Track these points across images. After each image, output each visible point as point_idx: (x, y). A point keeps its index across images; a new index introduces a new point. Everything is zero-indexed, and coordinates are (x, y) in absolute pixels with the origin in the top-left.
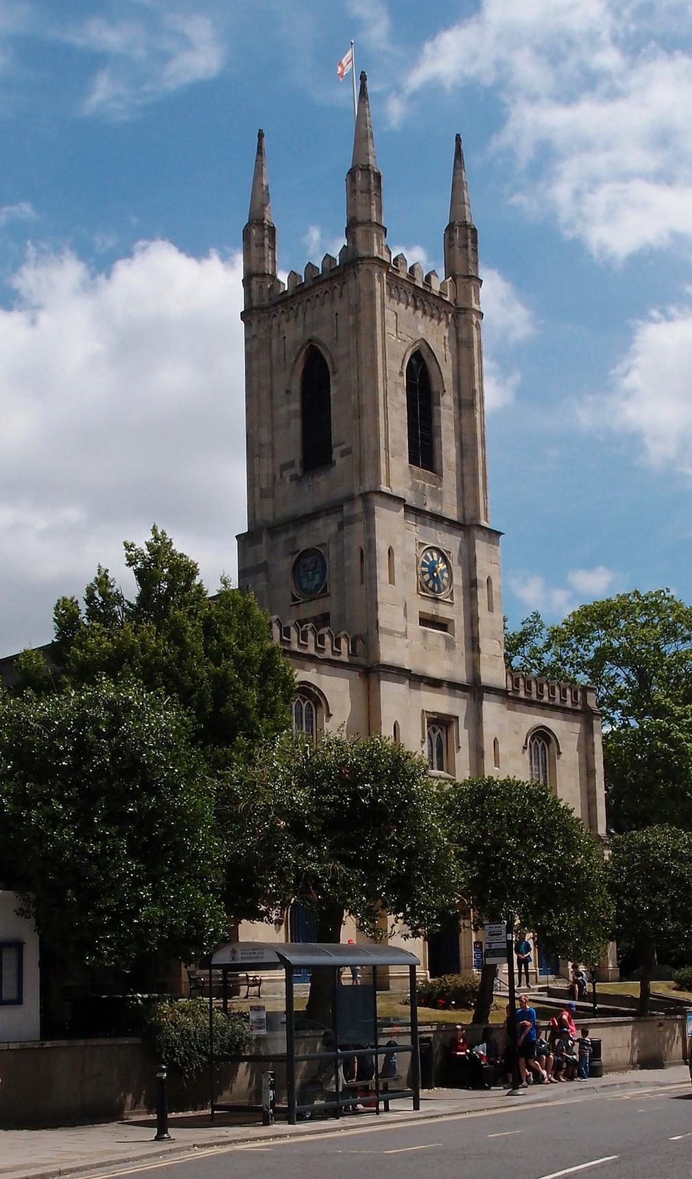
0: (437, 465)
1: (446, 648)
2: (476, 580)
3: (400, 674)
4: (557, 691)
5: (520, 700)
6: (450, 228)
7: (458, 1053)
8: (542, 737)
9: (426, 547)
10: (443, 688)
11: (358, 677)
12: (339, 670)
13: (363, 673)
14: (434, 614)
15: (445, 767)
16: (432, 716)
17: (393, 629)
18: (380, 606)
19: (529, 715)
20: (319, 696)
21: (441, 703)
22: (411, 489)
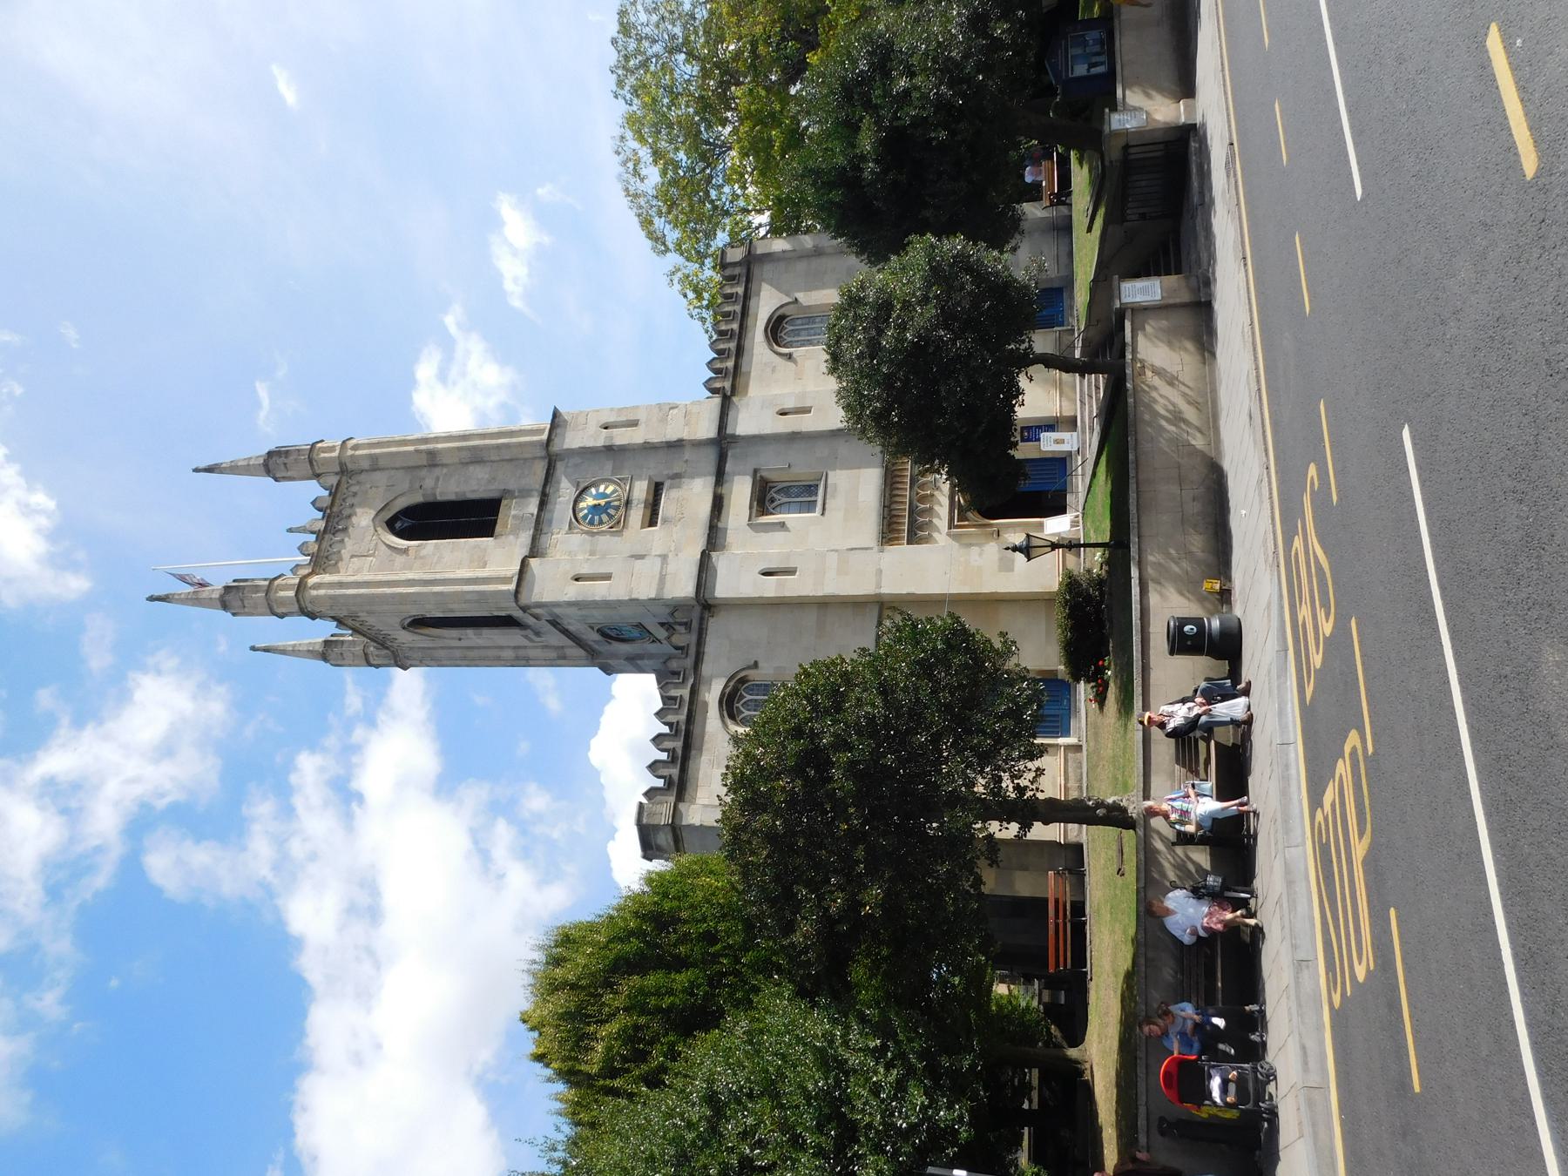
2: (604, 446)
3: (705, 567)
4: (728, 308)
5: (737, 367)
8: (777, 329)
9: (573, 520)
10: (723, 492)
11: (714, 618)
12: (751, 311)
13: (710, 612)
14: (643, 505)
15: (816, 483)
17: (658, 576)
18: (634, 596)
19: (755, 351)
20: (736, 679)
21: (740, 492)
22: (517, 536)
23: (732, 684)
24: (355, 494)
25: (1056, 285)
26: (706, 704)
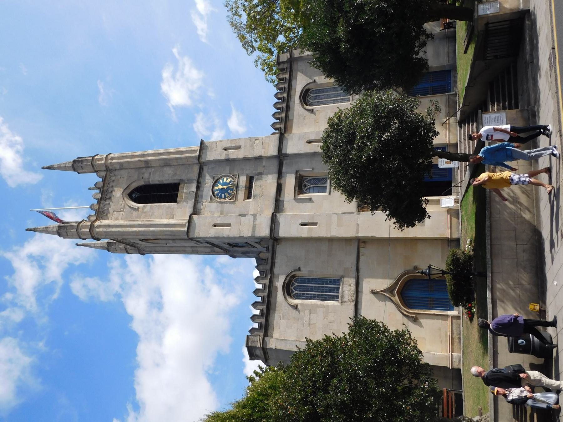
0: (176, 182)
1: (261, 179)
5: (287, 116)
6: (60, 235)
7: (507, 148)
9: (212, 196)
10: (282, 182)
13: (277, 242)
14: (244, 189)
16: (297, 191)
21: (290, 182)
23: (288, 278)
24: (113, 181)
25: (447, 69)
26: (276, 288)
